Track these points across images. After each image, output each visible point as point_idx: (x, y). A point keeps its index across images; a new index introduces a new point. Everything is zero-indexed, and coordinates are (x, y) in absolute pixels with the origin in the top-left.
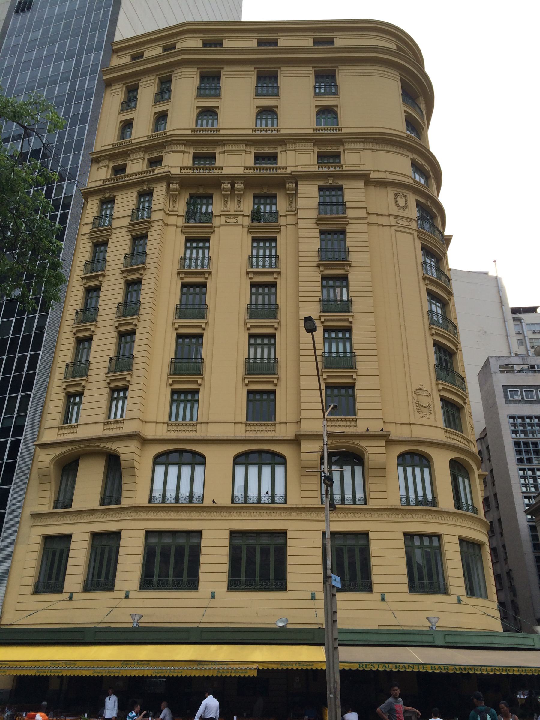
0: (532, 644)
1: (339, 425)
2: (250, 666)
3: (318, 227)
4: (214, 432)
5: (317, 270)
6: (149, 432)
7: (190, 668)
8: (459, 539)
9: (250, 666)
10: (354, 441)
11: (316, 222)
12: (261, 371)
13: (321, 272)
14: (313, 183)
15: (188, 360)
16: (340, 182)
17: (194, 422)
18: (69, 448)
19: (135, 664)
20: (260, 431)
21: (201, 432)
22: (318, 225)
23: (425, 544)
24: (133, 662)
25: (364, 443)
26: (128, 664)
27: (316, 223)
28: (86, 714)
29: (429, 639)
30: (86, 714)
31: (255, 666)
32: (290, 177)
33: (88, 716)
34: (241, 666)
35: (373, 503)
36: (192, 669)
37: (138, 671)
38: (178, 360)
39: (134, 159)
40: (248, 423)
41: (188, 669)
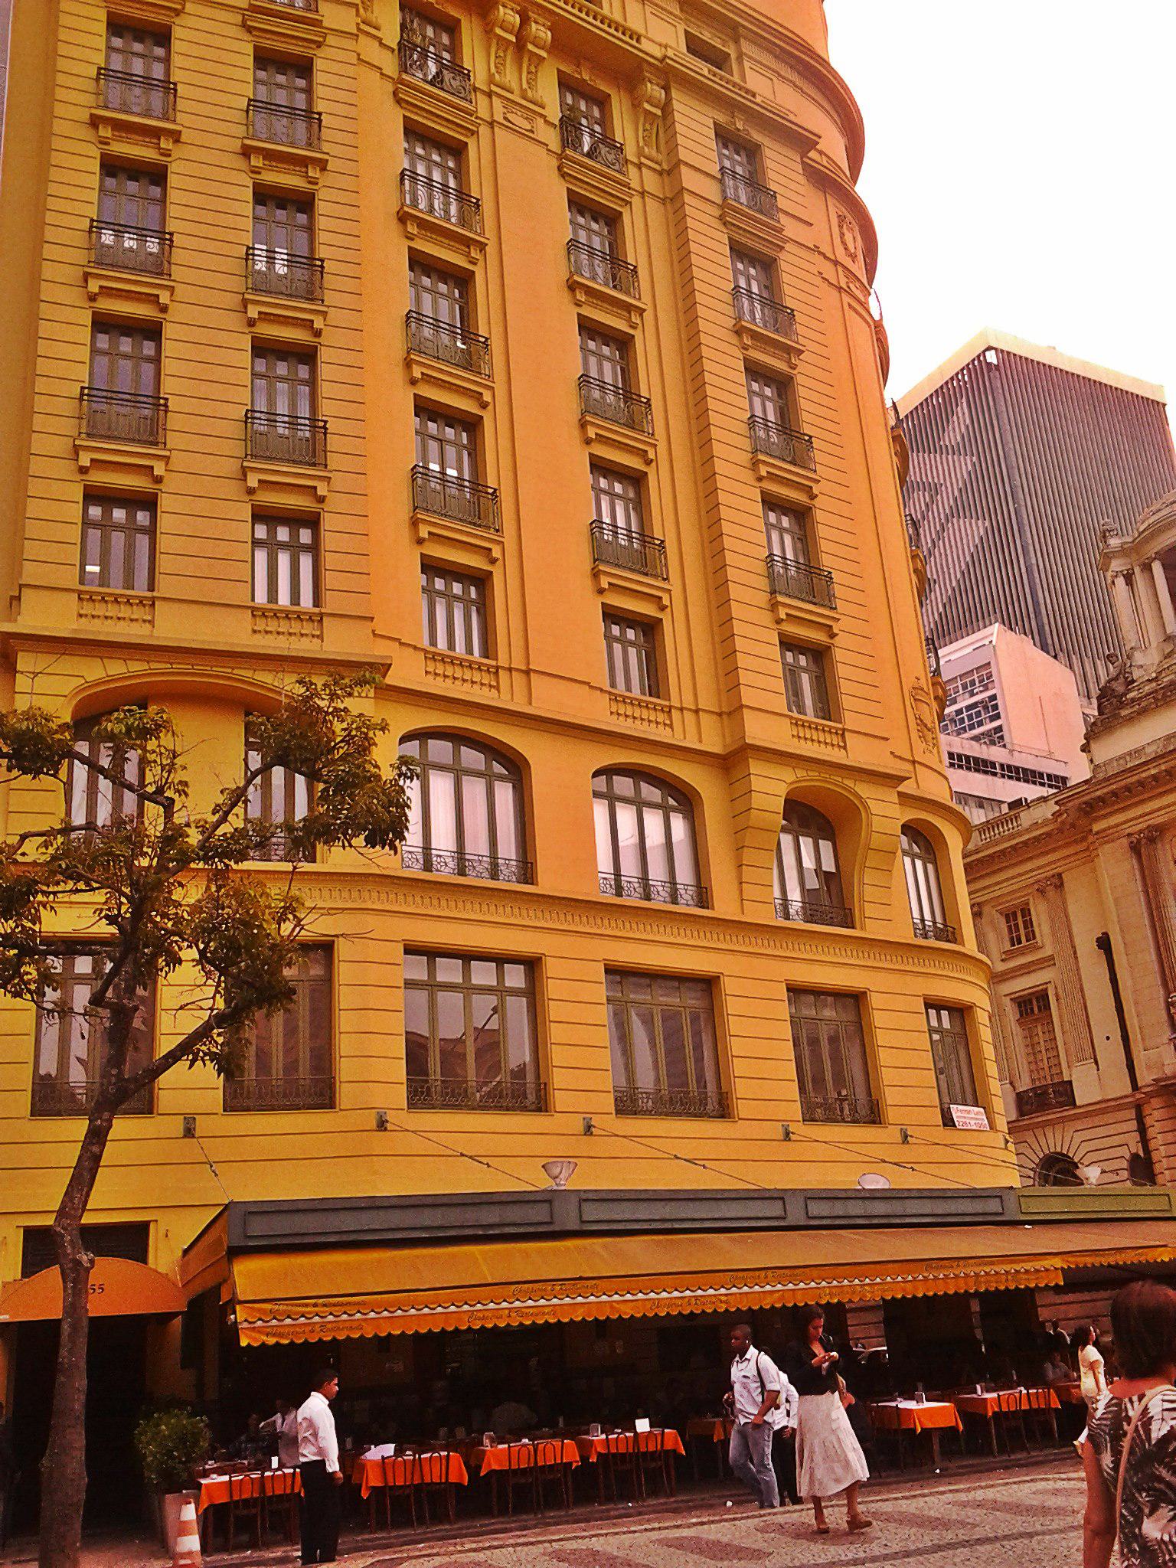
0: (779, 1212)
1: (268, 629)
2: (1048, 1263)
3: (247, 37)
4: (549, 700)
5: (240, 163)
6: (407, 672)
7: (921, 1277)
8: (788, 990)
9: (1048, 1263)
10: (846, 782)
11: (244, 21)
12: (109, 429)
13: (252, 172)
14: (706, 109)
15: (109, 395)
16: (757, 136)
17: (632, 695)
18: (136, 667)
19: (766, 1277)
20: (102, 619)
21: (509, 696)
22: (249, 30)
23: (507, 985)
24: (763, 1273)
25: (864, 790)
26: (364, 1303)
27: (244, 25)
28: (561, 1420)
29: (539, 1214)
30: (561, 1420)
31: (1058, 1263)
32: (657, 68)
33: (566, 1424)
34: (1029, 1266)
35: (546, 884)
36: (926, 1279)
37: (777, 1295)
38: (95, 393)
39: (665, 10)
40: (86, 592)
41: (905, 1281)
